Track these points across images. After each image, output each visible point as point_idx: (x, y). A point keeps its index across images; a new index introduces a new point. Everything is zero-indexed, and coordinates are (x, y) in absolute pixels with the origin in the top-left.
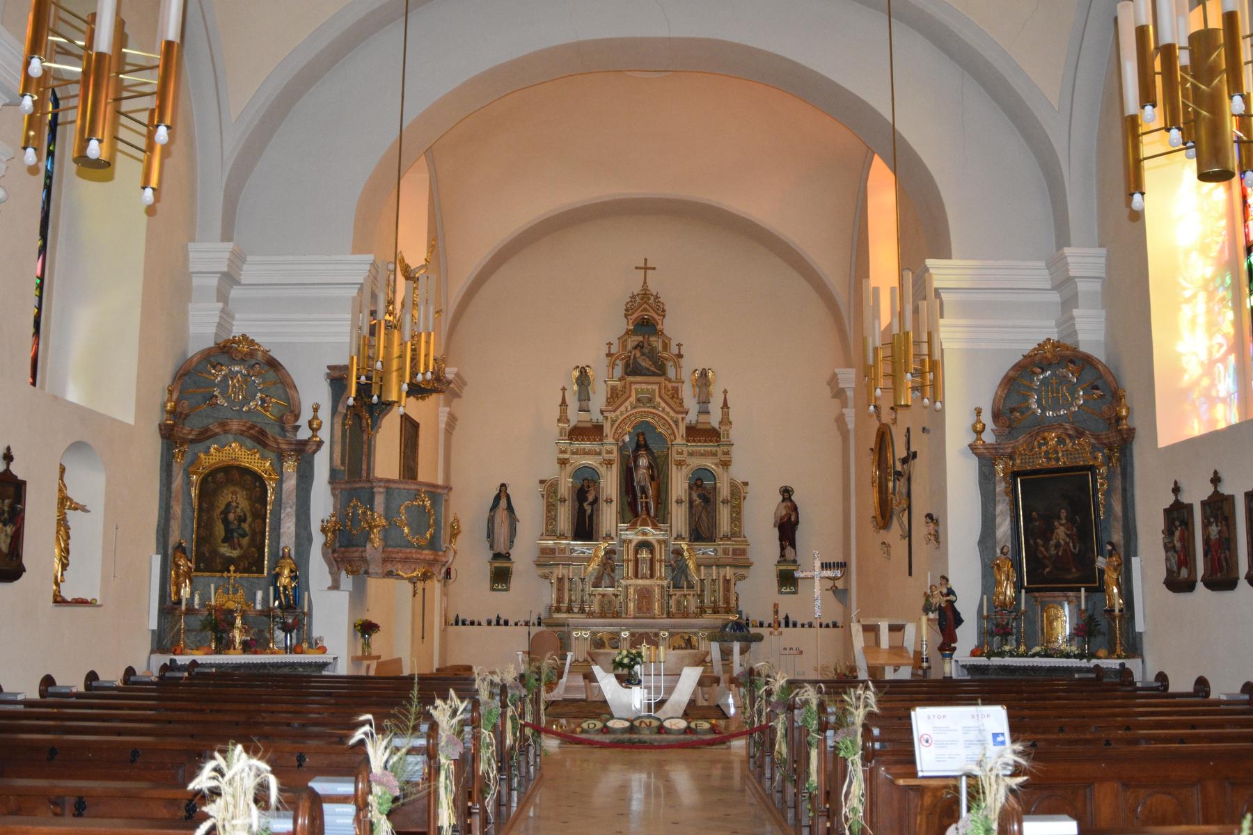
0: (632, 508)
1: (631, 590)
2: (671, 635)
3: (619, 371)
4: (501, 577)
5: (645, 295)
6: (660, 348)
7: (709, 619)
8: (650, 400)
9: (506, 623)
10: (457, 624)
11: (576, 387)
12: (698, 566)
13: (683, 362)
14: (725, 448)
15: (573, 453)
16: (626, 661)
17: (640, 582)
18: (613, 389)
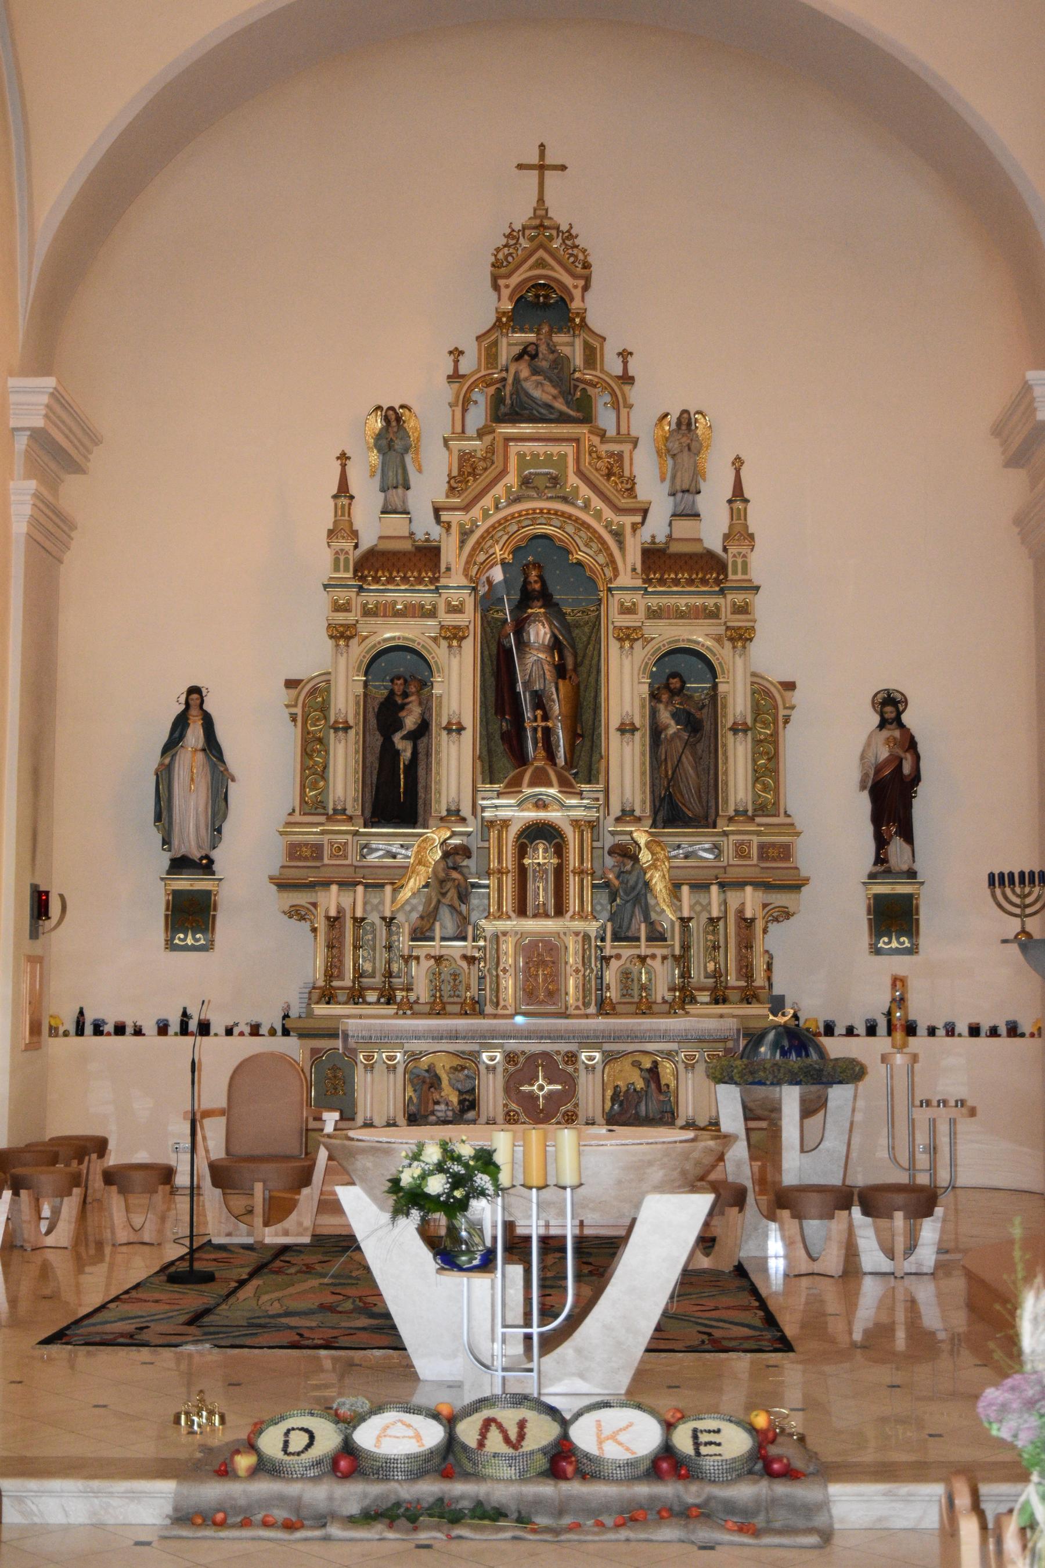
0: (509, 743)
1: (508, 947)
2: (610, 1058)
3: (478, 416)
4: (190, 916)
5: (541, 224)
6: (578, 360)
7: (706, 1019)
8: (555, 481)
9: (204, 1029)
10: (80, 1031)
11: (374, 457)
12: (675, 887)
13: (634, 394)
14: (739, 598)
15: (367, 612)
16: (436, 1185)
17: (531, 925)
18: (465, 458)
